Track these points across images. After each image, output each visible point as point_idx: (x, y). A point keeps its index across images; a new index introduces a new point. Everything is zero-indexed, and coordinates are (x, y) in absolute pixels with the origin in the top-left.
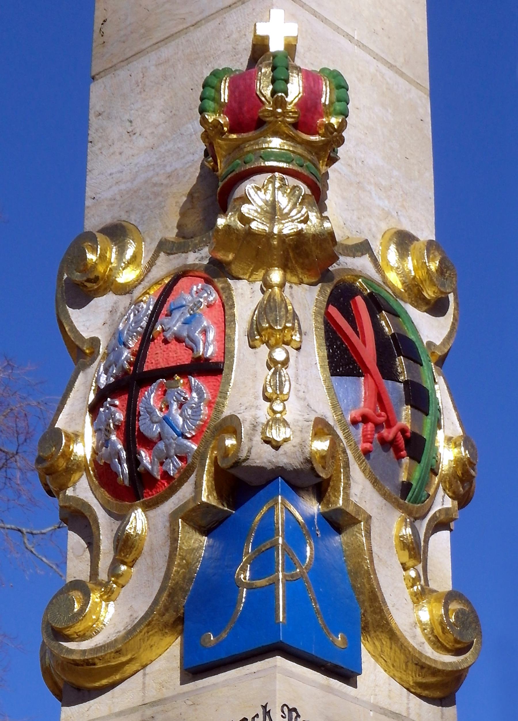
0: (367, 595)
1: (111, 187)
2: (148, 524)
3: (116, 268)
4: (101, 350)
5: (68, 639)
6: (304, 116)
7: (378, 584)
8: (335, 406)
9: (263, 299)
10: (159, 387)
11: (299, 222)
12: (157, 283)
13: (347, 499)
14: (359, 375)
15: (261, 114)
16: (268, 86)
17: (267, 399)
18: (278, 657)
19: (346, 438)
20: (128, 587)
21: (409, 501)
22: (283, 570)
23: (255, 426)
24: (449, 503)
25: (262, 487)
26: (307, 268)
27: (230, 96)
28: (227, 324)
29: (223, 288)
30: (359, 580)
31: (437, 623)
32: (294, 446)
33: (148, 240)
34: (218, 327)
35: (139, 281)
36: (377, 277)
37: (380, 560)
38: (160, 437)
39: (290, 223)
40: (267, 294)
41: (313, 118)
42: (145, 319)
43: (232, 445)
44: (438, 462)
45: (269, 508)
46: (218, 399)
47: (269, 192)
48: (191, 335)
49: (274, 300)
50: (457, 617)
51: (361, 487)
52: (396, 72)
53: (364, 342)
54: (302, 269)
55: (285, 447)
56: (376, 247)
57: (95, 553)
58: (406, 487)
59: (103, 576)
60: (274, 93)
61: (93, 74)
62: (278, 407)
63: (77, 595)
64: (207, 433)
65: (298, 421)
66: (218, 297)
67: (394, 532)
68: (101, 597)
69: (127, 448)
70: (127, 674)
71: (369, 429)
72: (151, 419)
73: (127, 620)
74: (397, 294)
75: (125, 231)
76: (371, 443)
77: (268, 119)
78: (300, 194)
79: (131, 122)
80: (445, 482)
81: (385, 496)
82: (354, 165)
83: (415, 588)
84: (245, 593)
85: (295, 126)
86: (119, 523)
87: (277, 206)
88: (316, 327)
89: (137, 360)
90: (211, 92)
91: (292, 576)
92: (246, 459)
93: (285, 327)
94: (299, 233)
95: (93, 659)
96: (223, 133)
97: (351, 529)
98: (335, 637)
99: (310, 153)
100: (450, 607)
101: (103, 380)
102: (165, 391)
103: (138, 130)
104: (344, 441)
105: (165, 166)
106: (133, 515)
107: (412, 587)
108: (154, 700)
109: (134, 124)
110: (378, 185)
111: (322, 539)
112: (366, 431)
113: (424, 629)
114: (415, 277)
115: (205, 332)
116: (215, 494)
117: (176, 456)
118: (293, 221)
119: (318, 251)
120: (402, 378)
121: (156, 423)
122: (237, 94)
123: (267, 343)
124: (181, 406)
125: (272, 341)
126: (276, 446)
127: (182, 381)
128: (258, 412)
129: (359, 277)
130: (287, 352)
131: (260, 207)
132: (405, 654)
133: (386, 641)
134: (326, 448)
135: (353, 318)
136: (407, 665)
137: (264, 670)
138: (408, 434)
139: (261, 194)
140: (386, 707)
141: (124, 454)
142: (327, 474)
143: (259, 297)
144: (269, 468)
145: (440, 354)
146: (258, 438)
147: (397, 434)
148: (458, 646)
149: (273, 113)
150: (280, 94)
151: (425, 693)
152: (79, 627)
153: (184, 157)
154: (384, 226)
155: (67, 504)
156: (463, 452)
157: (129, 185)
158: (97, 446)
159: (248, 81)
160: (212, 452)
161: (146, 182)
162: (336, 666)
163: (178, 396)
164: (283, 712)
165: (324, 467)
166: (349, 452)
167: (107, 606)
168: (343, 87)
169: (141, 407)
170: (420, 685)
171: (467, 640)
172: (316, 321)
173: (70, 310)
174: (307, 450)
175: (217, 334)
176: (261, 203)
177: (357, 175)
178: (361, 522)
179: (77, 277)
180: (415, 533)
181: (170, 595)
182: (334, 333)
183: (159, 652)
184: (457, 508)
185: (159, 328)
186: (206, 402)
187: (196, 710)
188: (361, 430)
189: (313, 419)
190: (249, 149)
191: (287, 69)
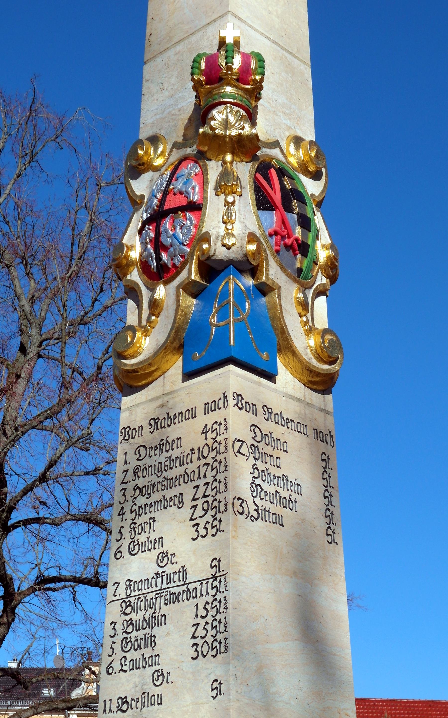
0: (279, 330)
1: (152, 117)
2: (166, 293)
3: (153, 158)
4: (145, 201)
5: (125, 358)
6: (242, 75)
7: (285, 324)
8: (260, 226)
9: (222, 170)
10: (171, 218)
11: (239, 129)
12: (172, 164)
13: (267, 277)
14: (273, 210)
15: (220, 75)
16: (224, 61)
17: (224, 223)
18: (231, 365)
19: (266, 243)
20: (156, 328)
21: (301, 279)
22: (233, 316)
23: (218, 237)
24: (325, 281)
25: (222, 271)
26: (245, 154)
27: (205, 66)
28: (204, 183)
29: (203, 165)
30: (275, 322)
31: (318, 346)
32: (238, 248)
33: (169, 143)
34: (200, 186)
35: (164, 164)
36: (283, 159)
37: (287, 311)
38: (171, 245)
39: (235, 130)
40: (224, 167)
41: (246, 76)
42: (165, 183)
43: (206, 248)
44: (317, 258)
45: (226, 282)
46: (200, 224)
47: (225, 115)
48: (187, 190)
49: (228, 170)
50: (329, 343)
51: (275, 270)
52: (293, 56)
53: (275, 193)
54: (242, 154)
55: (233, 248)
56: (283, 144)
57: (140, 310)
58: (300, 271)
59: (144, 323)
60: (226, 63)
61: (145, 60)
62: (229, 227)
63: (129, 333)
64: (195, 242)
65: (240, 234)
66: (200, 170)
67: (294, 296)
68: (142, 334)
69: (155, 252)
70: (155, 378)
71: (278, 238)
72: (167, 236)
73: (155, 347)
74: (294, 169)
75: (158, 139)
76: (280, 246)
77: (224, 77)
78: (240, 115)
79: (162, 84)
80: (322, 269)
81: (288, 275)
82: (271, 102)
83: (306, 327)
84: (214, 329)
85: (238, 80)
86: (151, 293)
87: (229, 121)
88: (250, 185)
89: (160, 205)
90: (197, 65)
91: (238, 319)
92: (213, 255)
93: (233, 184)
94: (240, 135)
95: (137, 369)
96: (202, 85)
97: (270, 294)
98: (262, 354)
99: (246, 94)
100: (325, 338)
101: (145, 217)
102: (174, 220)
103: (165, 88)
104: (265, 245)
105: (178, 105)
106: (158, 288)
107: (305, 326)
108: (168, 392)
109: (163, 84)
110: (284, 113)
111: (255, 299)
112: (277, 240)
113: (312, 350)
114: (304, 160)
115: (193, 188)
116: (199, 275)
117: (180, 255)
118: (236, 129)
119: (250, 144)
120: (296, 212)
121: (169, 237)
122: (209, 65)
123: (224, 193)
124: (181, 228)
125: (227, 192)
126: (229, 248)
127: (182, 215)
128: (220, 229)
129: (273, 159)
130: (234, 198)
131: (220, 122)
132: (301, 364)
133: (291, 357)
134: (255, 249)
135: (270, 180)
136: (302, 371)
137: (223, 373)
138: (300, 242)
139: (221, 115)
140: (292, 395)
141: (154, 255)
142: (256, 263)
143: (220, 169)
144: (225, 260)
145: (318, 200)
146: (219, 244)
147: (293, 241)
148: (331, 359)
149: (227, 74)
150: (229, 64)
151: (314, 387)
152: (130, 351)
153: (186, 100)
154: (288, 134)
155: (127, 284)
156: (329, 252)
157: (161, 115)
158: (141, 252)
159: (214, 58)
160: (197, 252)
161: (169, 114)
162: (263, 370)
163: (180, 223)
164: (234, 397)
165: (254, 259)
166: (268, 251)
167: (145, 339)
168: (262, 61)
169: (162, 230)
170: (311, 382)
171: (335, 356)
172: (250, 181)
173: (131, 181)
174: (244, 250)
175: (200, 189)
176: (221, 120)
177: (273, 107)
178: (274, 290)
179: (134, 163)
180: (305, 296)
181: (176, 332)
182: (259, 187)
183: (171, 364)
184: (329, 284)
185: (171, 187)
186: (194, 225)
187: (190, 397)
188: (274, 240)
189: (247, 233)
190: (215, 93)
191: (233, 52)
